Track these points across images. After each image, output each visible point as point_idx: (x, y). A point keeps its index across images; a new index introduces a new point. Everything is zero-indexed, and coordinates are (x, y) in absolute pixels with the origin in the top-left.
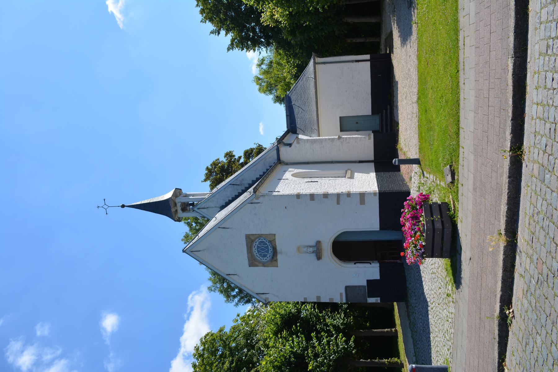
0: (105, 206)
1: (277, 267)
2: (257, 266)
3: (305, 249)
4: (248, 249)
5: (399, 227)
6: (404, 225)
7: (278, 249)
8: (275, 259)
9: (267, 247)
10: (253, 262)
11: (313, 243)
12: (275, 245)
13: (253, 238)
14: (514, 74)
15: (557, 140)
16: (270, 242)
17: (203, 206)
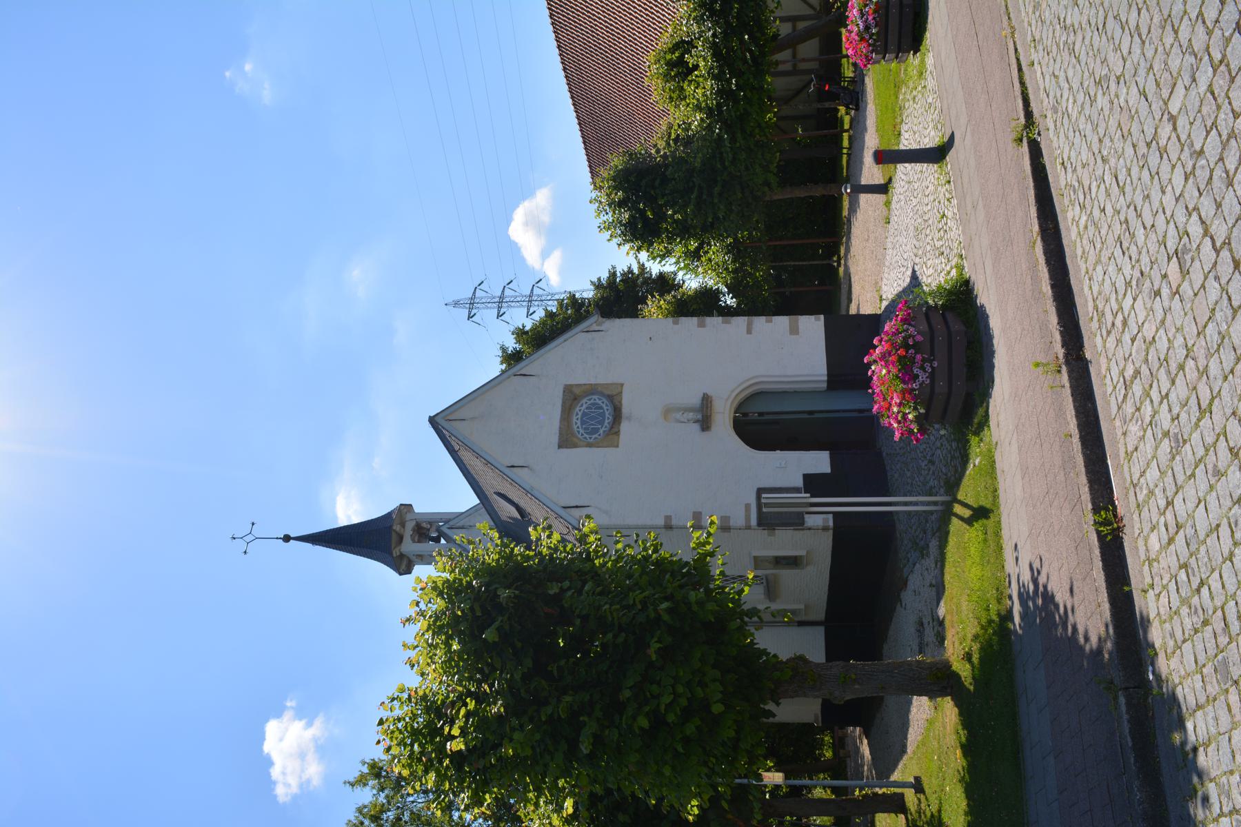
0: (249, 538)
1: (622, 385)
2: (575, 446)
3: (678, 415)
4: (563, 411)
5: (863, 382)
6: (875, 347)
7: (625, 410)
8: (615, 430)
9: (603, 415)
10: (572, 396)
11: (696, 400)
12: (620, 402)
13: (577, 391)
14: (1083, 440)
15: (1235, 672)
16: (610, 398)
17: (460, 524)
